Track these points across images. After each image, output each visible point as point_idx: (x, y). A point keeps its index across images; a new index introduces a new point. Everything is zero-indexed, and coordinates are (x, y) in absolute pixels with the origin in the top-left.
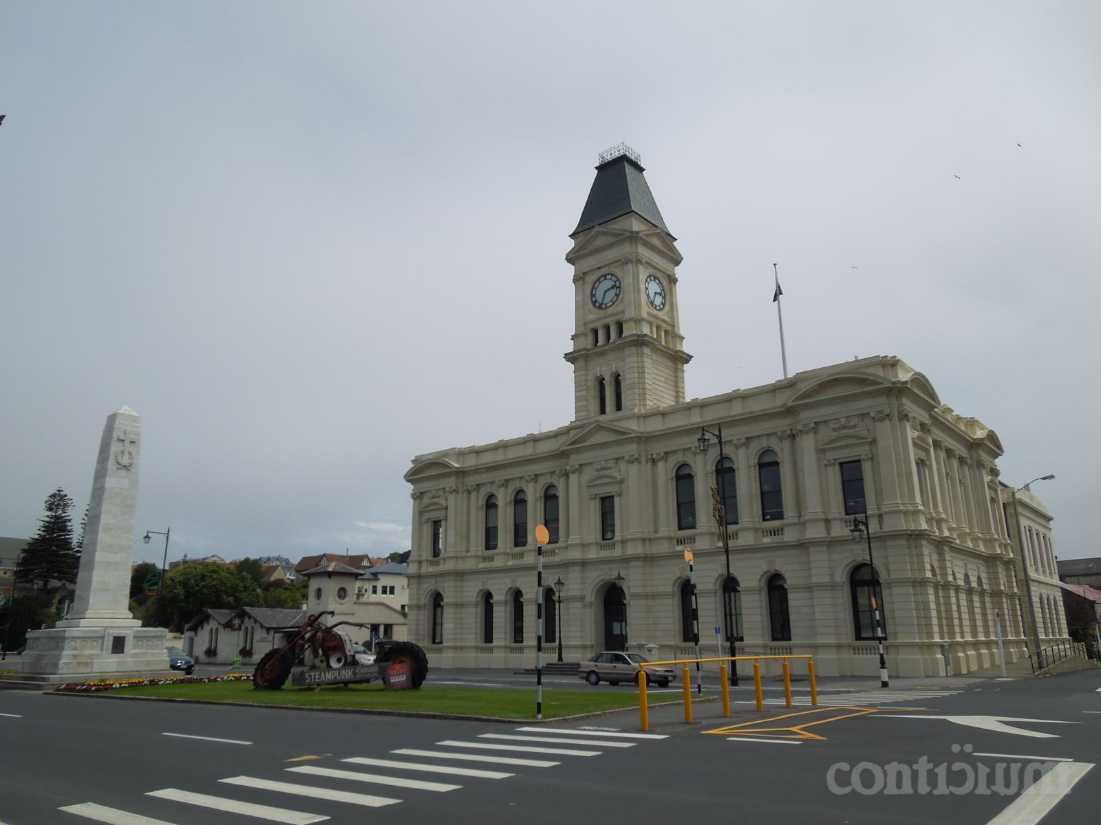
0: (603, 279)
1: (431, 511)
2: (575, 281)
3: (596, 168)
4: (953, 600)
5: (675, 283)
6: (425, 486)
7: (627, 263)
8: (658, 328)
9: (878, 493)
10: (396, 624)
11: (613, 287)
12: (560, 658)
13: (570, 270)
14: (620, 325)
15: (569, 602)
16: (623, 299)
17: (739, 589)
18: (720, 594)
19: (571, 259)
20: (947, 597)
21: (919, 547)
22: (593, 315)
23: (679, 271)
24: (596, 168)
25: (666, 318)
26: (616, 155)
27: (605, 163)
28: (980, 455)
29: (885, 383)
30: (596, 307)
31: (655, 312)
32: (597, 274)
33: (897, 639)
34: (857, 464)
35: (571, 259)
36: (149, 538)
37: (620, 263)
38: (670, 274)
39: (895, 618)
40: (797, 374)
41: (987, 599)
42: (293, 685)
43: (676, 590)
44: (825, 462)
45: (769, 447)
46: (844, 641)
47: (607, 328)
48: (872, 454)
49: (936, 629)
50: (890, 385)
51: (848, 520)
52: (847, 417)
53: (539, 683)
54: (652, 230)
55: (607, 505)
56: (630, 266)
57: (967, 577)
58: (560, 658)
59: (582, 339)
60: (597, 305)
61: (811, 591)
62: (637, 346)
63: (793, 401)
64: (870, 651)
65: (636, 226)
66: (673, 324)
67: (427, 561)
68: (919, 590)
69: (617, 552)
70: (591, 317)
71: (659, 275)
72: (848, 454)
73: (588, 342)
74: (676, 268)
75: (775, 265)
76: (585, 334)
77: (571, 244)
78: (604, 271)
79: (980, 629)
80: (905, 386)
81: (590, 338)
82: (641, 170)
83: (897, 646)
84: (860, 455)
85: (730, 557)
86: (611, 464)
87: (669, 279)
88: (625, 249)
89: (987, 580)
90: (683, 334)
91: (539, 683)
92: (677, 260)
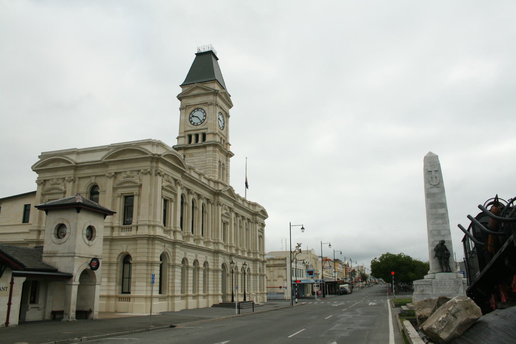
0: (196, 110)
1: (53, 194)
2: (181, 109)
3: (195, 54)
5: (229, 118)
6: (48, 175)
7: (211, 105)
8: (221, 138)
9: (138, 214)
10: (286, 270)
11: (193, 116)
12: (245, 299)
13: (178, 103)
14: (204, 135)
15: (136, 266)
16: (207, 122)
17: (131, 262)
18: (121, 265)
19: (180, 97)
20: (263, 279)
22: (190, 127)
23: (231, 111)
24: (195, 54)
25: (224, 134)
26: (207, 50)
27: (199, 53)
28: (219, 199)
29: (149, 154)
30: (191, 124)
31: (194, 128)
32: (192, 109)
33: (135, 294)
34: (132, 198)
35: (180, 97)
36: (304, 229)
37: (207, 104)
38: (228, 113)
39: (147, 282)
40: (111, 144)
43: (119, 260)
44: (117, 195)
45: (96, 183)
46: (113, 293)
47: (197, 136)
48: (139, 193)
49: (258, 289)
50: (152, 156)
51: (125, 228)
52: (131, 171)
54: (222, 91)
56: (212, 106)
58: (245, 299)
59: (183, 139)
60: (192, 123)
61: (110, 266)
62: (213, 146)
63: (105, 159)
64: (121, 299)
66: (227, 137)
67: (119, 227)
68: (150, 268)
69: (133, 233)
70: (188, 128)
71: (223, 113)
73: (184, 142)
74: (229, 110)
75: (246, 158)
76: (184, 137)
77: (180, 90)
78: (196, 107)
80: (160, 157)
81: (187, 139)
82: (217, 59)
83: (134, 297)
84: (133, 193)
85: (290, 250)
87: (226, 115)
88: (210, 98)
89: (252, 267)
90: (230, 143)
92: (230, 106)
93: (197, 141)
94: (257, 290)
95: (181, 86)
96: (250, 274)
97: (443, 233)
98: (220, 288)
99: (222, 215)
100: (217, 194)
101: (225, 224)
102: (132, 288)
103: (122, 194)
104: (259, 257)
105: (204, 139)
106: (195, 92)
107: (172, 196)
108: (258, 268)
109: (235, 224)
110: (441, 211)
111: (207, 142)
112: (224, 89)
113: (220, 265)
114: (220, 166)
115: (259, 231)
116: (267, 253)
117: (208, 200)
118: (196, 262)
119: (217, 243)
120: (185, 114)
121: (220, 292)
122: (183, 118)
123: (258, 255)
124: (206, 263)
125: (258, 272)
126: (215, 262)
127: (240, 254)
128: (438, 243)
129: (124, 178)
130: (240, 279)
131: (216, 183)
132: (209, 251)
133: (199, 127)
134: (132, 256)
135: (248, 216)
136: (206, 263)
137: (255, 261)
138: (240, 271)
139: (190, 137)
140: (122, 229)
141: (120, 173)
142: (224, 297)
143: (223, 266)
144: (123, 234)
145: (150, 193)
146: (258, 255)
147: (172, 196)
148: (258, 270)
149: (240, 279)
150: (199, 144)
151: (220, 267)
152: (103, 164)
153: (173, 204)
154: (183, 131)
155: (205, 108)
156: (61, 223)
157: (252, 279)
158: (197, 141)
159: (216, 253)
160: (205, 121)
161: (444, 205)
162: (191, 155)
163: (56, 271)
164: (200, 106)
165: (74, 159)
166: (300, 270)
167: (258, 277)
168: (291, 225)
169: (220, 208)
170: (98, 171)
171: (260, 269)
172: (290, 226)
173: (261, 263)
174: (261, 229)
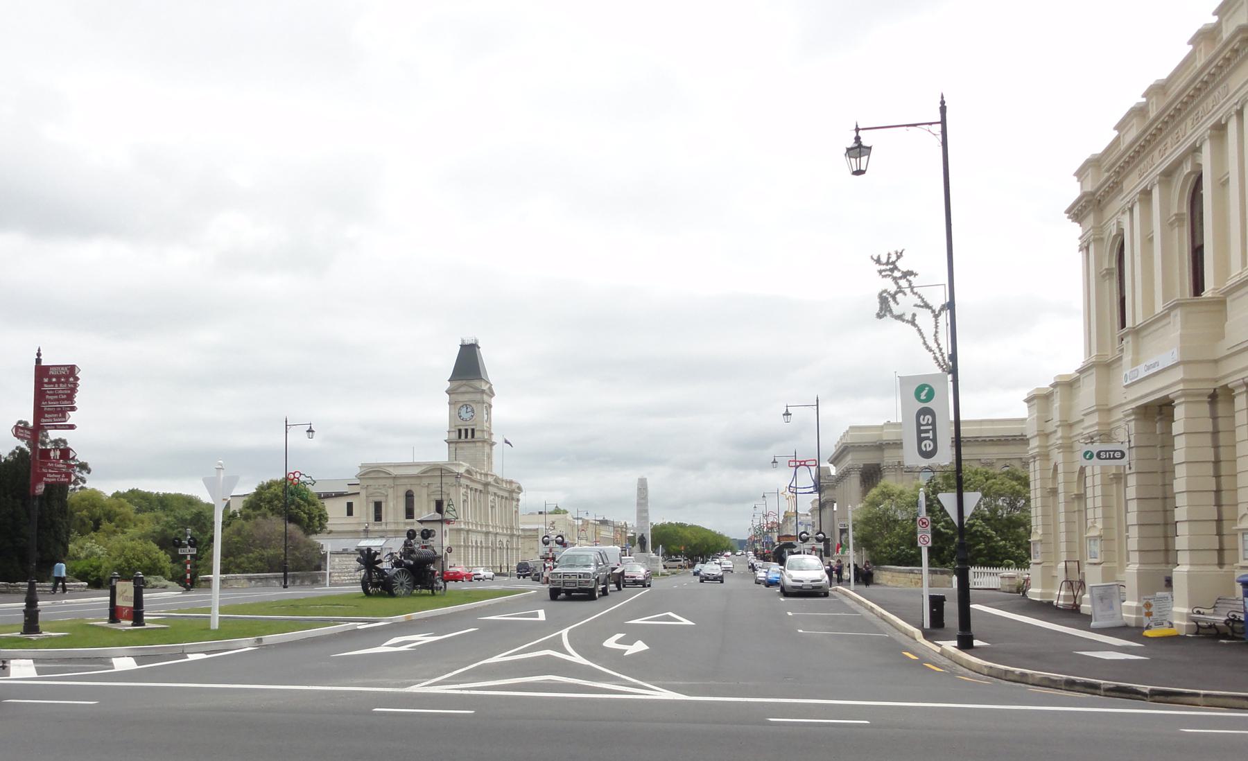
4: (470, 552)
20: (468, 550)
21: (460, 534)
22: (459, 422)
31: (463, 423)
32: (461, 404)
36: (313, 431)
41: (484, 550)
42: (537, 612)
47: (466, 430)
53: (31, 623)
55: (378, 506)
57: (476, 541)
65: (485, 387)
69: (383, 527)
72: (378, 499)
73: (455, 436)
79: (479, 562)
81: (457, 432)
86: (381, 487)
88: (478, 397)
91: (31, 623)
93: (466, 437)
94: (468, 563)
95: (449, 380)
96: (482, 547)
97: (645, 528)
104: (491, 530)
105: (473, 436)
106: (463, 389)
108: (490, 540)
110: (645, 515)
115: (463, 495)
116: (1084, 613)
117: (481, 491)
119: (487, 526)
120: (455, 408)
122: (453, 413)
123: (490, 527)
126: (487, 540)
131: (486, 475)
132: (479, 532)
133: (468, 423)
139: (460, 431)
140: (375, 525)
144: (376, 528)
145: (855, 601)
146: (490, 527)
152: (417, 477)
154: (453, 425)
155: (474, 406)
157: (484, 552)
158: (466, 437)
159: (487, 533)
160: (474, 417)
161: (646, 511)
162: (462, 448)
164: (468, 403)
165: (395, 472)
167: (515, 551)
170: (413, 481)
171: (464, 539)
173: (493, 535)
174: (466, 492)
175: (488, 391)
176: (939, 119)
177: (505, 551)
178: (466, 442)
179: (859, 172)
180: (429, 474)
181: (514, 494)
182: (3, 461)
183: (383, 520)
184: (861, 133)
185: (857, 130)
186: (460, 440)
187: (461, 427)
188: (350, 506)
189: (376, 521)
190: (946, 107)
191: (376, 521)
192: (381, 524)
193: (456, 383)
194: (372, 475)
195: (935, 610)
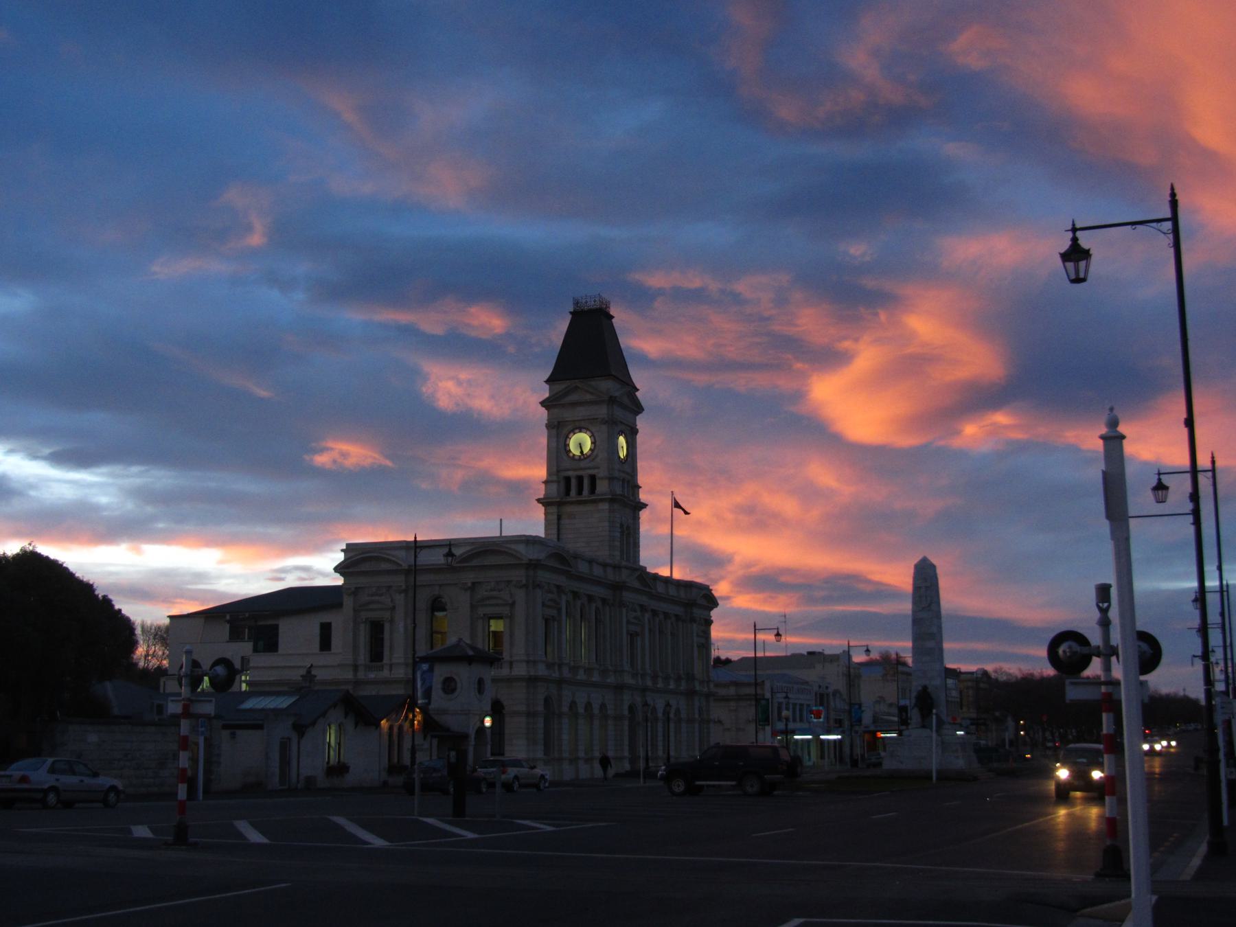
14: (593, 479)
32: (570, 427)
69: (385, 673)
81: (563, 484)
93: (580, 492)
95: (547, 381)
98: (626, 748)
99: (628, 622)
100: (617, 587)
101: (632, 636)
102: (507, 748)
103: (484, 615)
106: (574, 397)
107: (554, 612)
109: (650, 630)
110: (930, 644)
111: (598, 495)
112: (628, 385)
113: (626, 707)
114: (622, 533)
115: (698, 636)
117: (604, 601)
118: (588, 706)
121: (626, 754)
124: (603, 707)
125: (697, 716)
127: (660, 685)
128: (920, 688)
129: (486, 591)
130: (660, 729)
131: (617, 567)
134: (505, 703)
135: (679, 610)
136: (603, 707)
137: (691, 694)
138: (660, 715)
141: (479, 583)
142: (633, 760)
143: (632, 709)
144: (372, 676)
147: (554, 612)
148: (696, 711)
149: (660, 729)
150: (585, 497)
151: (626, 712)
153: (556, 623)
156: (449, 676)
158: (580, 492)
159: (619, 688)
163: (448, 730)
166: (801, 705)
168: (757, 628)
169: (624, 610)
172: (1174, 219)
175: (626, 400)
176: (1169, 215)
177: (660, 725)
178: (579, 503)
179: (1078, 280)
180: (475, 563)
181: (625, 594)
182: (4, 562)
183: (386, 661)
184: (1079, 234)
185: (1074, 230)
186: (569, 499)
187: (570, 473)
188: (326, 630)
189: (372, 661)
190: (1177, 201)
191: (372, 661)
192: (381, 668)
193: (560, 387)
194: (365, 567)
195: (1147, 731)
